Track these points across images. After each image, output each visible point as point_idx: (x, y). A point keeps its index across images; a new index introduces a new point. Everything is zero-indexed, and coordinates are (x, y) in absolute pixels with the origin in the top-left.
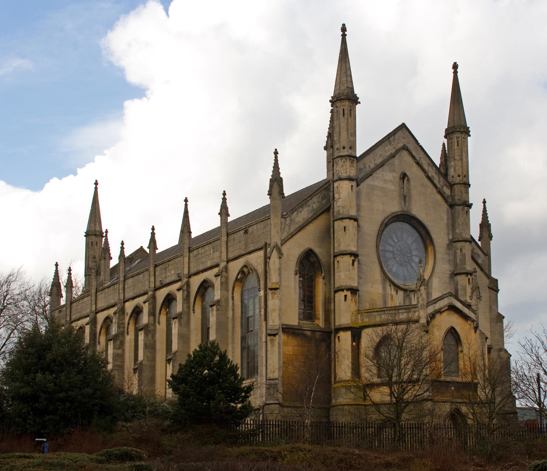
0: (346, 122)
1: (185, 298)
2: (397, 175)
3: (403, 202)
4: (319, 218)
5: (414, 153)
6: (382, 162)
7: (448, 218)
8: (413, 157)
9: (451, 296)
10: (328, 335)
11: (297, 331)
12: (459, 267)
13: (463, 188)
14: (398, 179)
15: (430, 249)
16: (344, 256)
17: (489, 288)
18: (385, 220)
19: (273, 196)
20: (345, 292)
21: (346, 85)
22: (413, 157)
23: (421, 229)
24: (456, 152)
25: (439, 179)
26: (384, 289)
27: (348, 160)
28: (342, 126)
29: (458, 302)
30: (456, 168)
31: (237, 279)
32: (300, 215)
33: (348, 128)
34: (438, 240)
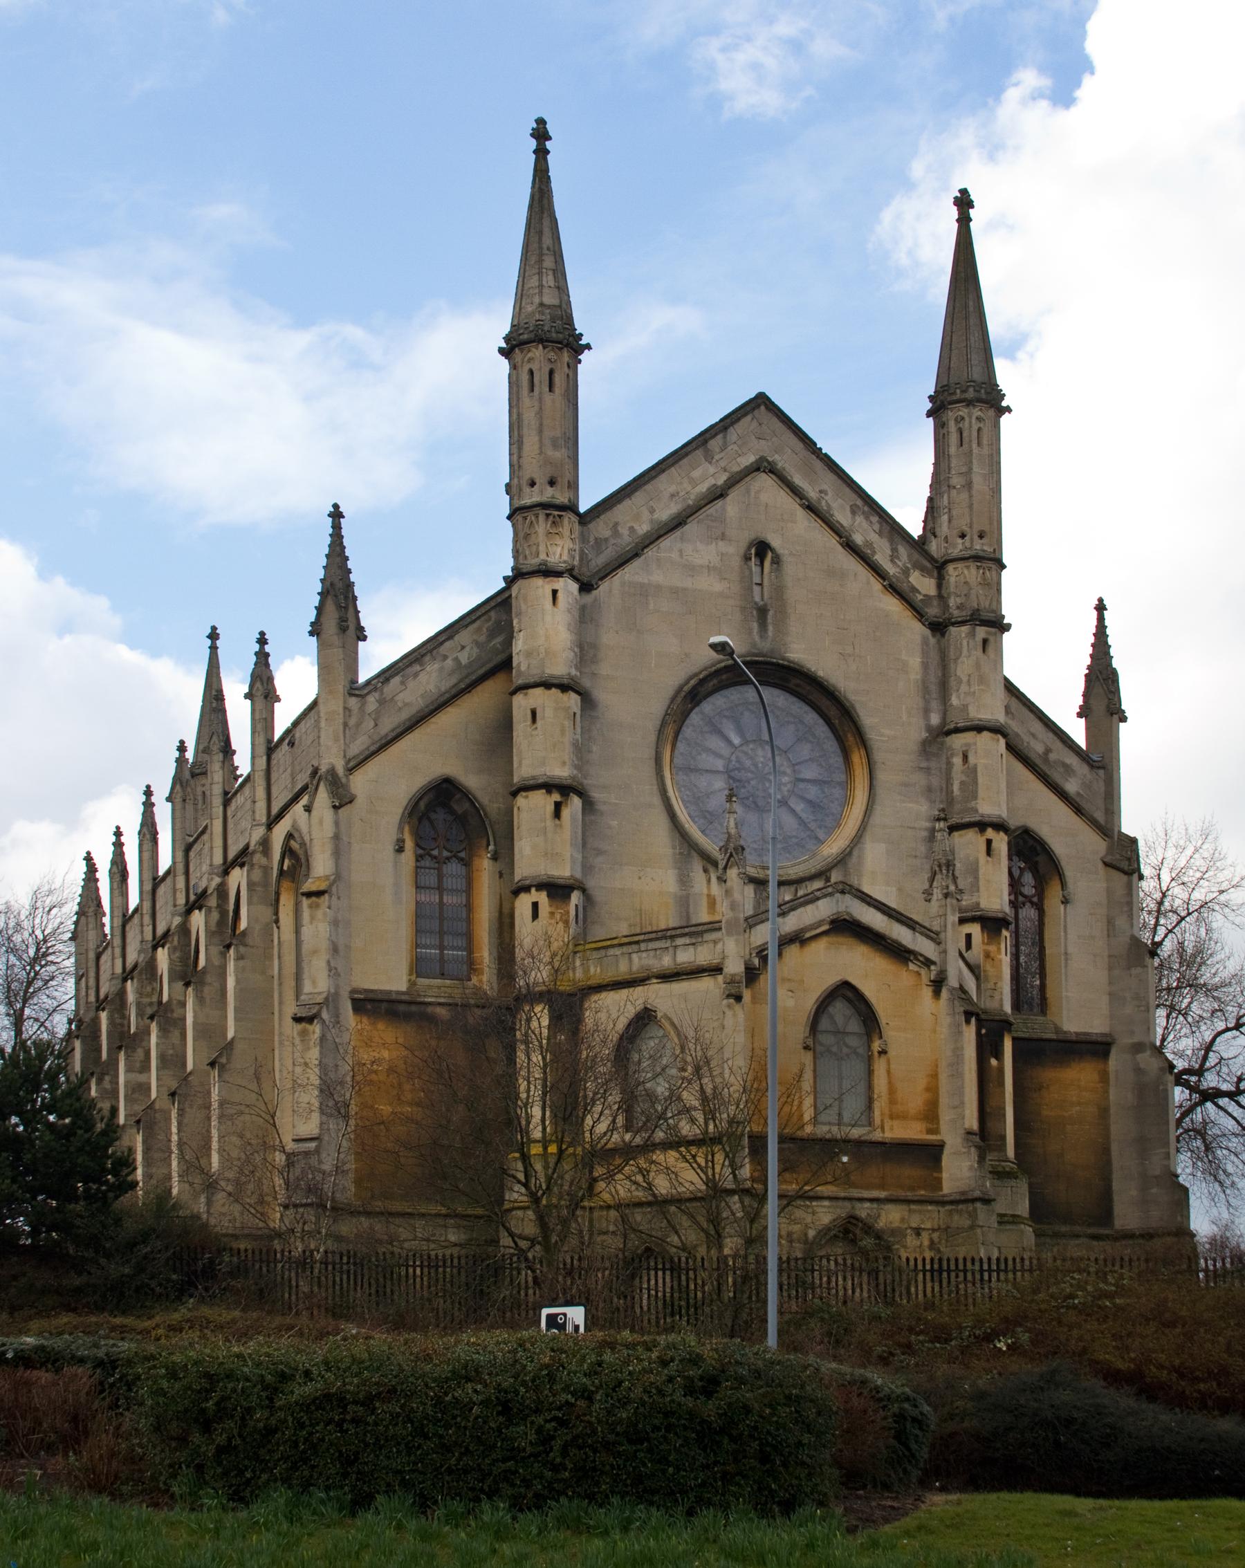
0: (536, 408)
1: (213, 928)
2: (734, 550)
3: (755, 625)
4: (479, 688)
5: (798, 480)
6: (679, 515)
7: (925, 666)
8: (795, 491)
9: (843, 892)
10: (498, 1021)
11: (402, 1008)
12: (957, 807)
13: (971, 573)
14: (736, 561)
15: (857, 758)
16: (531, 794)
17: (1106, 864)
18: (687, 682)
19: (323, 636)
20: (535, 895)
21: (537, 300)
22: (795, 491)
23: (824, 703)
24: (954, 462)
25: (894, 550)
26: (684, 880)
27: (542, 518)
28: (526, 422)
29: (872, 910)
30: (954, 513)
31: (281, 872)
32: (411, 684)
33: (541, 425)
34: (887, 732)
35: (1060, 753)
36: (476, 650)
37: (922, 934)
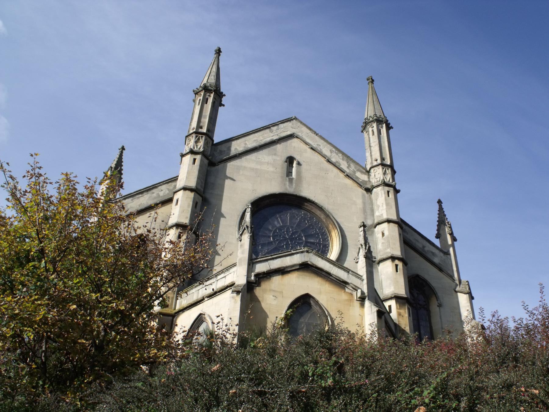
35: (429, 247)
36: (167, 192)
37: (352, 275)
